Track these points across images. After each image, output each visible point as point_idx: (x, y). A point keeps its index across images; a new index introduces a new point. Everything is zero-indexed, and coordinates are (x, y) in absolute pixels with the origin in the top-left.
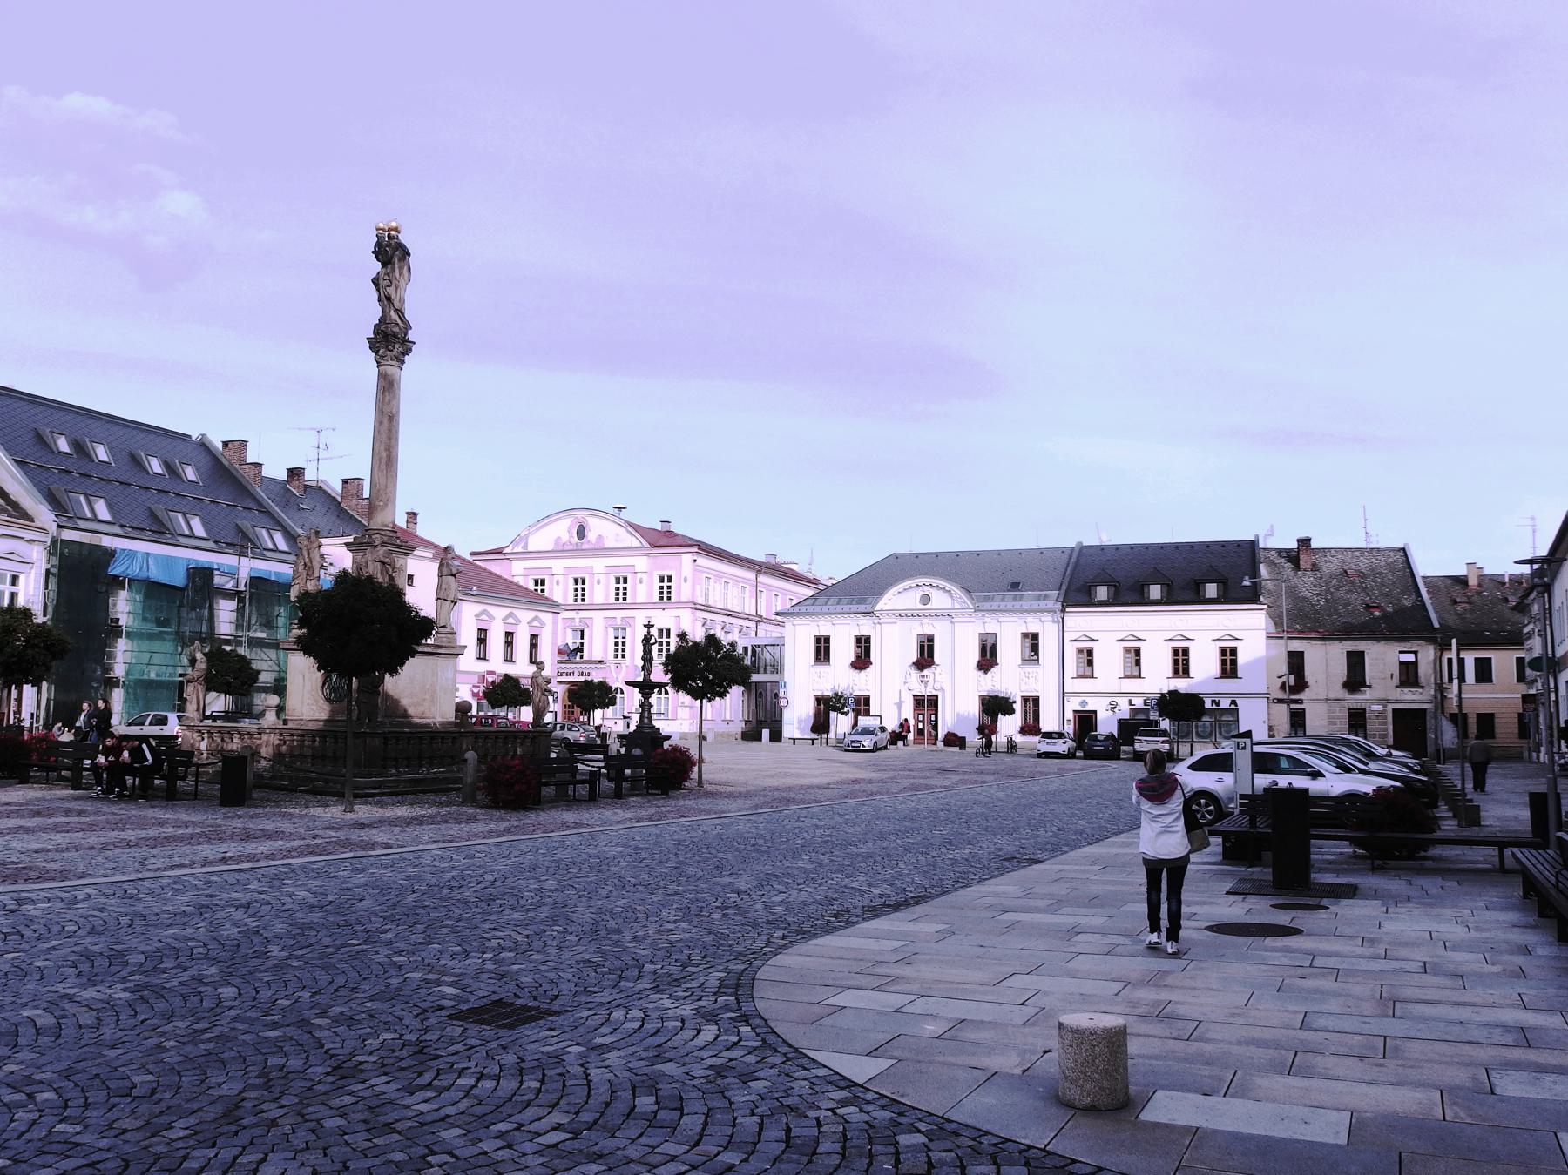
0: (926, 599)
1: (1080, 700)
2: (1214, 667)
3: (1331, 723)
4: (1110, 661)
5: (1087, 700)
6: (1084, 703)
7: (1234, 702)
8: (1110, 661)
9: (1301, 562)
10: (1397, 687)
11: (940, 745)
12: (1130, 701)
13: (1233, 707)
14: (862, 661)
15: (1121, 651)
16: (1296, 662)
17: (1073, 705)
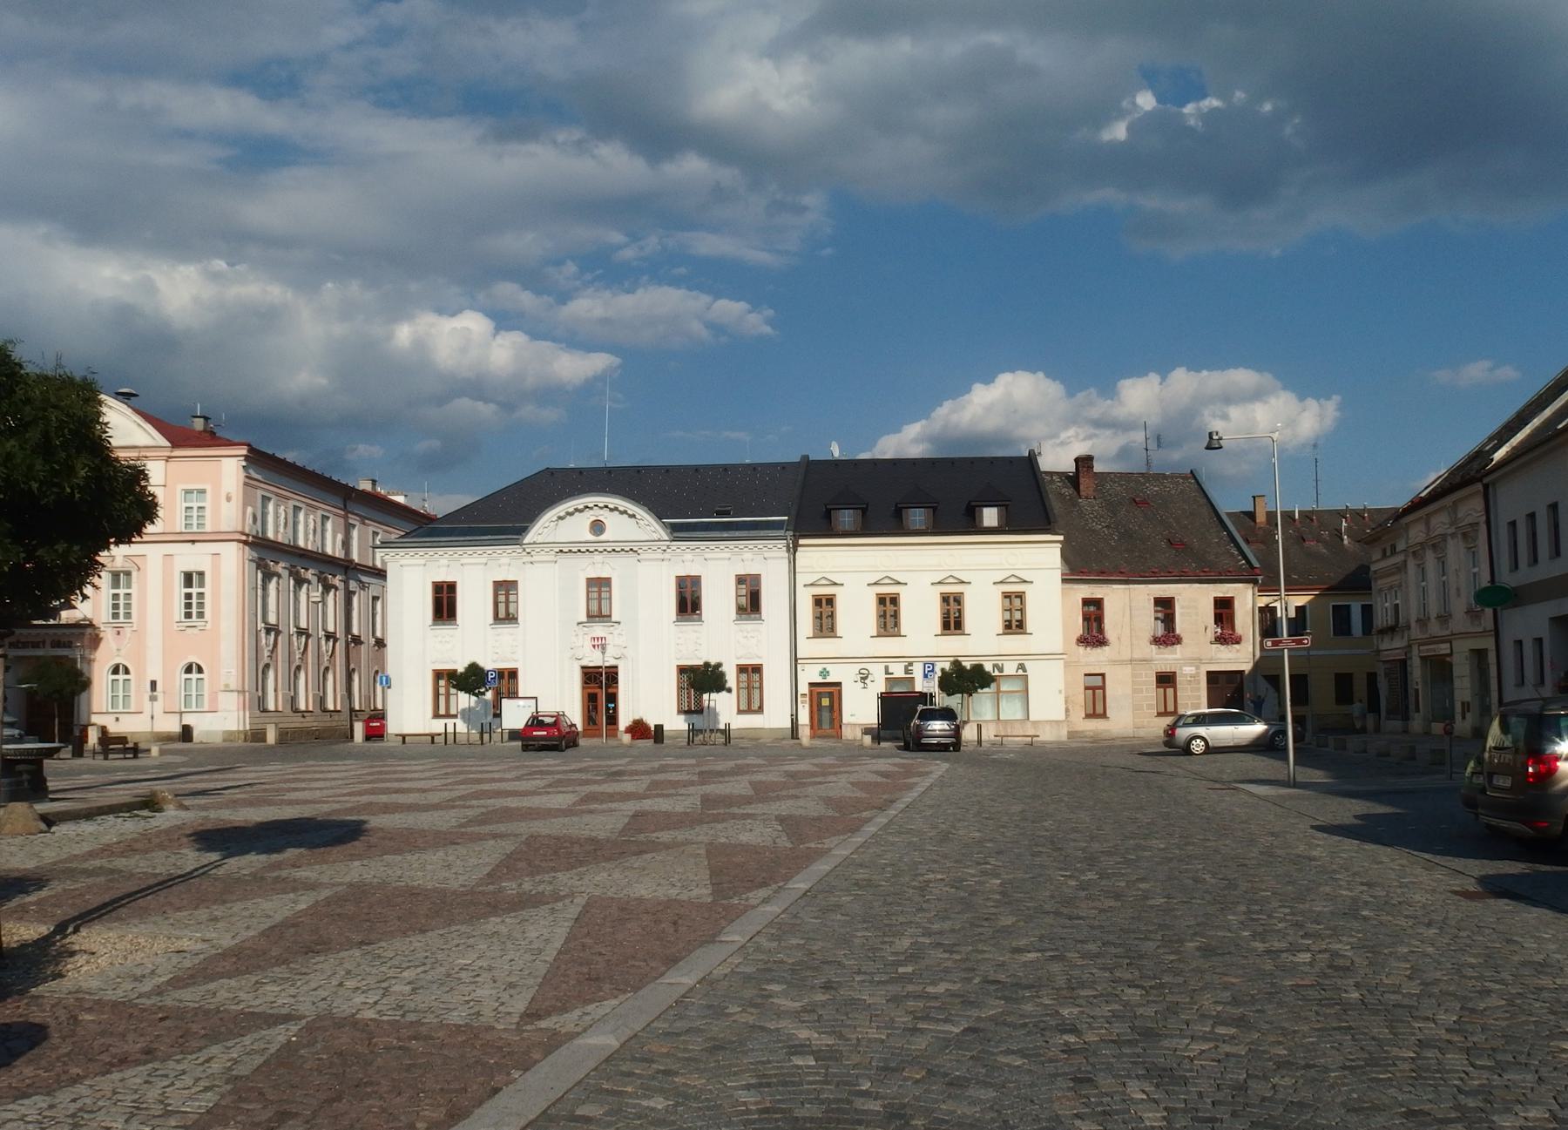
0: (597, 527)
1: (820, 668)
2: (997, 621)
3: (1135, 691)
4: (856, 614)
5: (829, 667)
6: (824, 673)
7: (1022, 667)
8: (856, 614)
9: (1082, 487)
10: (1211, 643)
11: (627, 738)
12: (887, 668)
13: (1020, 672)
14: (505, 616)
15: (1000, 596)
16: (1093, 613)
17: (809, 674)
